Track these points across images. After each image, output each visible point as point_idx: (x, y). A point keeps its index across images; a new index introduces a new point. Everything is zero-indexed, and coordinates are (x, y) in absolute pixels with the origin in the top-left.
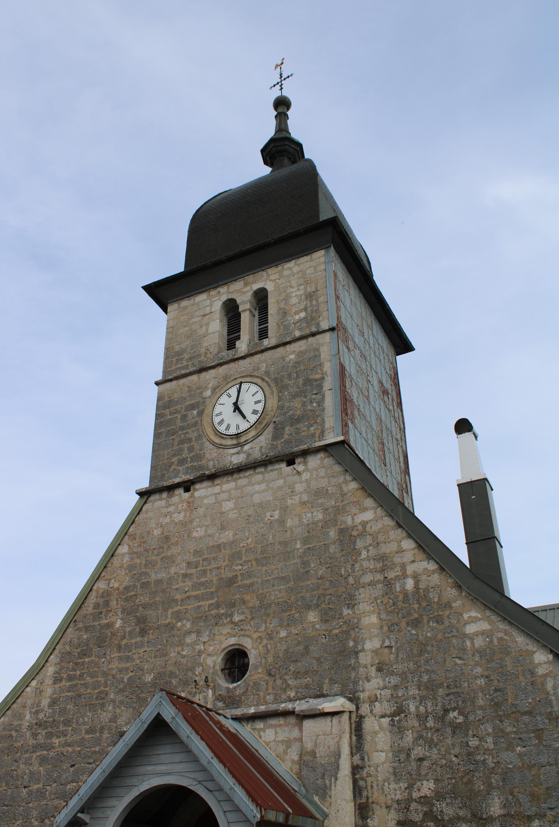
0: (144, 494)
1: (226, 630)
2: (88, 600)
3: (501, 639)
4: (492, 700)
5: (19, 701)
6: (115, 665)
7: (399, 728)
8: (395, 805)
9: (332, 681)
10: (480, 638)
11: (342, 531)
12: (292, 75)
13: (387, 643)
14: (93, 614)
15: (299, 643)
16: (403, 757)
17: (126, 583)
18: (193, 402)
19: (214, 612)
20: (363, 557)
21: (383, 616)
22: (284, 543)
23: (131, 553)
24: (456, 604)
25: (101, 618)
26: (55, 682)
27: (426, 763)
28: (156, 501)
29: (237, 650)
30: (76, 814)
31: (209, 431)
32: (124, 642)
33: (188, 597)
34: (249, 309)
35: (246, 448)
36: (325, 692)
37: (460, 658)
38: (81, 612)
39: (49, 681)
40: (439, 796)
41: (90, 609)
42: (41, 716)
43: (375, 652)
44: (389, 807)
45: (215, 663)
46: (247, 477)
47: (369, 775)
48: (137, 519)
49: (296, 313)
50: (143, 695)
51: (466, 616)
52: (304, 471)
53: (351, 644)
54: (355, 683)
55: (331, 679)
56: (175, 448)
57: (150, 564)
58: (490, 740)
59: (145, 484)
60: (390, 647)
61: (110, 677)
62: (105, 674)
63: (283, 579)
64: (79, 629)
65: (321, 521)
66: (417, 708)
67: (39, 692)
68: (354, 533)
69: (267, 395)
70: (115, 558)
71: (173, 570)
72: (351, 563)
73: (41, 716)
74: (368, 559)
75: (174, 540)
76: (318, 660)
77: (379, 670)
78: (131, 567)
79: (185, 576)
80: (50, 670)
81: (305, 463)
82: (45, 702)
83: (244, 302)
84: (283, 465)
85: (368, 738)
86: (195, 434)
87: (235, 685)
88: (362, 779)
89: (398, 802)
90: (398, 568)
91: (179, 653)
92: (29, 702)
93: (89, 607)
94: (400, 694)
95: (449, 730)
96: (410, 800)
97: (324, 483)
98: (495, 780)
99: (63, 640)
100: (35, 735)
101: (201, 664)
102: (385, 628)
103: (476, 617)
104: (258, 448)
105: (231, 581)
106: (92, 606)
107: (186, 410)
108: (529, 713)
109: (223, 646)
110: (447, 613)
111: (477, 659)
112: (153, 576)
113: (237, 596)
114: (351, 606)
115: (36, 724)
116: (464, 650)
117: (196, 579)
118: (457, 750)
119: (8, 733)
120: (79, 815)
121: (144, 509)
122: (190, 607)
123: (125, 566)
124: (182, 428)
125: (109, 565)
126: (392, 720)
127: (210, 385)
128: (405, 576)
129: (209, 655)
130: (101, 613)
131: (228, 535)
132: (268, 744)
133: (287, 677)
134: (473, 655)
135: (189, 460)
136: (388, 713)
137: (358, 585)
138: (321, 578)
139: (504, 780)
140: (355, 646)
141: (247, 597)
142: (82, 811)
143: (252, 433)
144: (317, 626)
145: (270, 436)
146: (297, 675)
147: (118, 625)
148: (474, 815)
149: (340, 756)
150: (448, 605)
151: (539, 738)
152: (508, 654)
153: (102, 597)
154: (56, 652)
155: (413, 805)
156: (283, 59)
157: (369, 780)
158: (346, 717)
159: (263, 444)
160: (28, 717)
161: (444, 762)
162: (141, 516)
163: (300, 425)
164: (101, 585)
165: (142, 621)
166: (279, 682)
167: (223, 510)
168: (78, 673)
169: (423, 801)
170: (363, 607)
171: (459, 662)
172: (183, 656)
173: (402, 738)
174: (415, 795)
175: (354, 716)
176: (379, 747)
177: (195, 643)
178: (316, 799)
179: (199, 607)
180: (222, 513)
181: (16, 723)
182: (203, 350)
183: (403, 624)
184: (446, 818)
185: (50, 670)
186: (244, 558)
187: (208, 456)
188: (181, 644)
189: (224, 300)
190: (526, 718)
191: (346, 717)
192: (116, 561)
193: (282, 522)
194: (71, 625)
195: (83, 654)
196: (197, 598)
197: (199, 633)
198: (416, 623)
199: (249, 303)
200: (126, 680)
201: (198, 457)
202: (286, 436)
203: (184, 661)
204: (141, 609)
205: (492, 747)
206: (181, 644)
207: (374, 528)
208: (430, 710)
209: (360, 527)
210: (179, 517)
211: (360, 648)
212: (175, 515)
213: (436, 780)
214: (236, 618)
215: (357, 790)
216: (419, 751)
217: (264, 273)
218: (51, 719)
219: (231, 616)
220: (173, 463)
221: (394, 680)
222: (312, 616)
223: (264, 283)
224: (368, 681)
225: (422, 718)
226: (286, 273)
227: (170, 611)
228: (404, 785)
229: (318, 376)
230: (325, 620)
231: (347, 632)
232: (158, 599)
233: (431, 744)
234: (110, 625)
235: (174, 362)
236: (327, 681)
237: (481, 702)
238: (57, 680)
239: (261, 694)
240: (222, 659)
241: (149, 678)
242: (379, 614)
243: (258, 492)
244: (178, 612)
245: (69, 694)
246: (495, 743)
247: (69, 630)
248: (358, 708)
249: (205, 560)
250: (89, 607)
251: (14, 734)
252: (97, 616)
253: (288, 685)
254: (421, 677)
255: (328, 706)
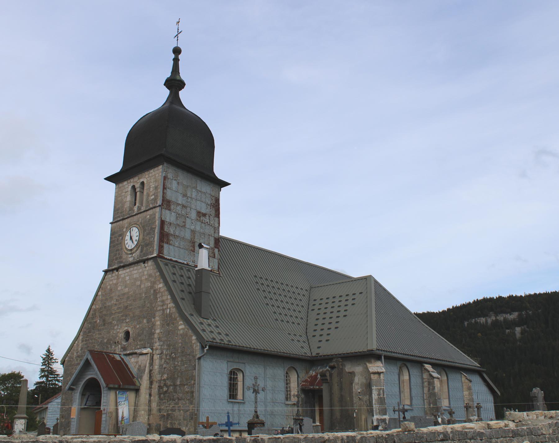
0: (106, 272)
1: (125, 325)
2: (90, 313)
3: (186, 331)
4: (182, 350)
5: (73, 348)
6: (97, 336)
7: (161, 358)
8: (158, 381)
9: (148, 343)
10: (182, 330)
11: (155, 291)
12: (182, 31)
13: (161, 331)
14: (92, 317)
15: (141, 330)
16: (161, 367)
17: (100, 307)
18: (120, 233)
19: (122, 318)
20: (158, 300)
21: (161, 322)
22: (140, 294)
23: (102, 295)
24: (178, 319)
25: (93, 319)
26: (82, 342)
27: (166, 369)
28: (109, 274)
29: (127, 331)
30: (70, 387)
31: (124, 247)
32: (100, 328)
33: (116, 312)
34: (139, 191)
35: (134, 255)
36: (146, 346)
37: (177, 337)
38: (89, 317)
39: (80, 342)
40: (167, 379)
41: (91, 316)
42: (79, 354)
43: (158, 334)
44: (157, 382)
45: (121, 336)
46: (132, 267)
47: (153, 372)
48: (104, 282)
49: (152, 196)
50: (104, 347)
51: (179, 323)
52: (147, 266)
53: (153, 331)
54: (153, 343)
55: (148, 343)
56: (115, 253)
57: (106, 299)
58: (180, 363)
59: (106, 268)
60: (162, 332)
61: (96, 340)
62: (95, 339)
63: (139, 307)
64: (88, 323)
65: (149, 286)
66: (166, 352)
67: (78, 345)
68: (157, 292)
69: (140, 233)
70: (97, 297)
71: (112, 302)
72: (156, 302)
73: (79, 354)
74: (159, 301)
75: (113, 290)
76: (145, 336)
77: (159, 340)
78: (102, 300)
79: (116, 304)
80: (81, 337)
81: (148, 263)
82: (80, 349)
83: (138, 188)
84: (142, 264)
85: (154, 361)
86: (120, 248)
87: (126, 343)
88: (152, 374)
89: (159, 380)
90: (166, 305)
91: (113, 332)
92: (76, 349)
93: (90, 316)
94: (162, 348)
95: (172, 359)
96: (161, 380)
97: (152, 272)
98: (179, 374)
99: (84, 327)
100: (77, 360)
101: (118, 336)
102: (161, 326)
103: (182, 324)
104: (136, 256)
105: (126, 307)
106: (91, 314)
107: (119, 237)
108: (189, 355)
109: (124, 330)
110: (175, 322)
111: (180, 337)
112: (107, 304)
113: (128, 313)
114: (154, 318)
115: (77, 356)
116: (178, 334)
117: (118, 306)
118: (172, 366)
119: (70, 359)
120: (71, 386)
121: (106, 278)
122: (116, 316)
123: (100, 300)
124: (117, 245)
125: (96, 299)
126: (160, 356)
127: (125, 227)
128: (167, 308)
129: (120, 333)
130: (94, 317)
131: (126, 290)
132: (132, 362)
133: (138, 341)
134: (180, 336)
135: (118, 258)
136: (159, 353)
137: (157, 311)
138: (148, 307)
139: (181, 374)
140: (154, 332)
141: (130, 313)
142: (71, 385)
143: (135, 249)
144: (146, 324)
145: (140, 251)
146: (140, 341)
147: (98, 322)
148: (174, 384)
149: (146, 367)
150: (176, 319)
151: (190, 362)
152: (187, 336)
153: (94, 311)
154: (82, 331)
155: (162, 381)
156: (180, 19)
157: (153, 374)
158: (149, 355)
159: (138, 254)
160: (75, 354)
161: (169, 369)
162: (105, 281)
163: (148, 247)
164: (94, 307)
165: (104, 320)
166: (136, 343)
167: (126, 280)
168: (88, 339)
169: (164, 380)
170: (157, 318)
171: (176, 338)
172: (114, 333)
173: (161, 361)
174: (163, 378)
175: (152, 354)
176: (156, 364)
177: (117, 329)
178: (139, 380)
179: (118, 316)
180: (126, 281)
181: (72, 356)
182: (125, 209)
183: (165, 325)
184: (168, 385)
185: (81, 337)
186: (130, 299)
187: (123, 257)
188: (114, 329)
189: (132, 186)
190: (188, 356)
191: (149, 355)
192: (98, 298)
193: (140, 286)
194: (86, 321)
195: (89, 332)
196: (119, 313)
197: (118, 325)
198: (168, 325)
199: (139, 188)
200: (100, 341)
201: (121, 257)
202: (144, 251)
203: (114, 335)
204: (104, 316)
205: (180, 365)
206: (114, 329)
207: (162, 290)
208: (168, 353)
209: (159, 290)
210: (115, 282)
211: (155, 332)
212: (114, 281)
213: (168, 374)
214: (127, 321)
215: (150, 377)
216: (164, 366)
217: (144, 174)
218: (81, 355)
219: (126, 320)
220: (114, 259)
221: (162, 343)
222: (145, 321)
223: (144, 179)
224: (156, 343)
225: (166, 355)
226: (150, 175)
227: (111, 318)
228: (160, 375)
229: (154, 227)
230: (148, 323)
231: (152, 327)
232: (108, 313)
233: (167, 363)
234: (96, 322)
235: (116, 214)
236: (147, 343)
237: (179, 351)
238: (82, 341)
239: (132, 347)
240: (124, 334)
241: (105, 341)
242: (160, 321)
243: (135, 274)
244: (113, 318)
245: (85, 346)
246: (181, 364)
247: (85, 323)
248: (153, 352)
249: (120, 299)
250: (90, 316)
251: (72, 360)
252: (93, 318)
253: (138, 344)
254: (167, 342)
255: (145, 351)
